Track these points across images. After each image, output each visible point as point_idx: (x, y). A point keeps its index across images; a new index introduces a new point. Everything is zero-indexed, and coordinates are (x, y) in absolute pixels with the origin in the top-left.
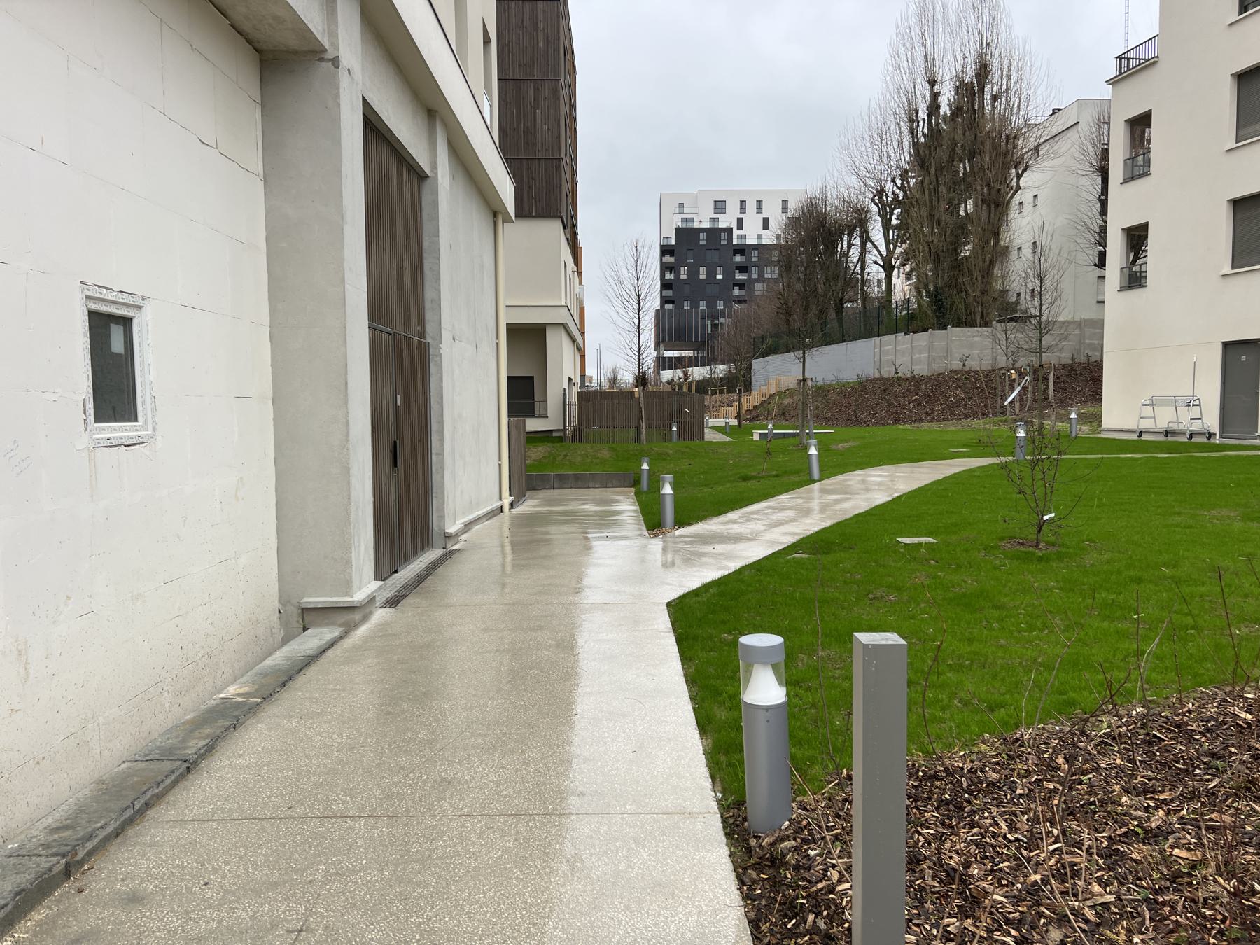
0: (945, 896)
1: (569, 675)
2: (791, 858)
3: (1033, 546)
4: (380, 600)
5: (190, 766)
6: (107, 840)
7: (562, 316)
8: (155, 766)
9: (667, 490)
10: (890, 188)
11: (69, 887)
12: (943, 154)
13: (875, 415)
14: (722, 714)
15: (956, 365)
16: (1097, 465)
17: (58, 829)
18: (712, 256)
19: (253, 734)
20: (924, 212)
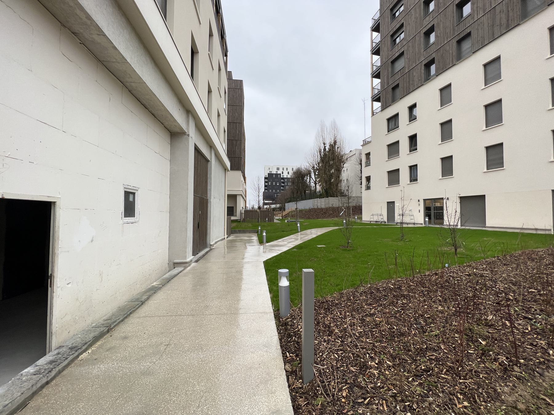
0: (324, 331)
1: (240, 279)
2: (290, 323)
3: (347, 247)
4: (193, 261)
5: (143, 303)
6: (119, 322)
7: (241, 193)
8: (133, 303)
9: (264, 234)
10: (315, 166)
11: (108, 335)
12: (327, 159)
13: (313, 217)
14: (275, 288)
15: (331, 206)
16: (360, 229)
17: (107, 320)
18: (276, 180)
19: (159, 295)
20: (323, 172)
